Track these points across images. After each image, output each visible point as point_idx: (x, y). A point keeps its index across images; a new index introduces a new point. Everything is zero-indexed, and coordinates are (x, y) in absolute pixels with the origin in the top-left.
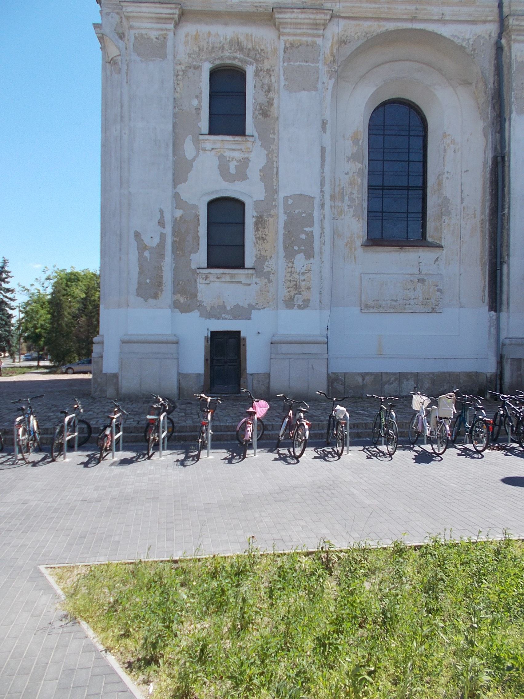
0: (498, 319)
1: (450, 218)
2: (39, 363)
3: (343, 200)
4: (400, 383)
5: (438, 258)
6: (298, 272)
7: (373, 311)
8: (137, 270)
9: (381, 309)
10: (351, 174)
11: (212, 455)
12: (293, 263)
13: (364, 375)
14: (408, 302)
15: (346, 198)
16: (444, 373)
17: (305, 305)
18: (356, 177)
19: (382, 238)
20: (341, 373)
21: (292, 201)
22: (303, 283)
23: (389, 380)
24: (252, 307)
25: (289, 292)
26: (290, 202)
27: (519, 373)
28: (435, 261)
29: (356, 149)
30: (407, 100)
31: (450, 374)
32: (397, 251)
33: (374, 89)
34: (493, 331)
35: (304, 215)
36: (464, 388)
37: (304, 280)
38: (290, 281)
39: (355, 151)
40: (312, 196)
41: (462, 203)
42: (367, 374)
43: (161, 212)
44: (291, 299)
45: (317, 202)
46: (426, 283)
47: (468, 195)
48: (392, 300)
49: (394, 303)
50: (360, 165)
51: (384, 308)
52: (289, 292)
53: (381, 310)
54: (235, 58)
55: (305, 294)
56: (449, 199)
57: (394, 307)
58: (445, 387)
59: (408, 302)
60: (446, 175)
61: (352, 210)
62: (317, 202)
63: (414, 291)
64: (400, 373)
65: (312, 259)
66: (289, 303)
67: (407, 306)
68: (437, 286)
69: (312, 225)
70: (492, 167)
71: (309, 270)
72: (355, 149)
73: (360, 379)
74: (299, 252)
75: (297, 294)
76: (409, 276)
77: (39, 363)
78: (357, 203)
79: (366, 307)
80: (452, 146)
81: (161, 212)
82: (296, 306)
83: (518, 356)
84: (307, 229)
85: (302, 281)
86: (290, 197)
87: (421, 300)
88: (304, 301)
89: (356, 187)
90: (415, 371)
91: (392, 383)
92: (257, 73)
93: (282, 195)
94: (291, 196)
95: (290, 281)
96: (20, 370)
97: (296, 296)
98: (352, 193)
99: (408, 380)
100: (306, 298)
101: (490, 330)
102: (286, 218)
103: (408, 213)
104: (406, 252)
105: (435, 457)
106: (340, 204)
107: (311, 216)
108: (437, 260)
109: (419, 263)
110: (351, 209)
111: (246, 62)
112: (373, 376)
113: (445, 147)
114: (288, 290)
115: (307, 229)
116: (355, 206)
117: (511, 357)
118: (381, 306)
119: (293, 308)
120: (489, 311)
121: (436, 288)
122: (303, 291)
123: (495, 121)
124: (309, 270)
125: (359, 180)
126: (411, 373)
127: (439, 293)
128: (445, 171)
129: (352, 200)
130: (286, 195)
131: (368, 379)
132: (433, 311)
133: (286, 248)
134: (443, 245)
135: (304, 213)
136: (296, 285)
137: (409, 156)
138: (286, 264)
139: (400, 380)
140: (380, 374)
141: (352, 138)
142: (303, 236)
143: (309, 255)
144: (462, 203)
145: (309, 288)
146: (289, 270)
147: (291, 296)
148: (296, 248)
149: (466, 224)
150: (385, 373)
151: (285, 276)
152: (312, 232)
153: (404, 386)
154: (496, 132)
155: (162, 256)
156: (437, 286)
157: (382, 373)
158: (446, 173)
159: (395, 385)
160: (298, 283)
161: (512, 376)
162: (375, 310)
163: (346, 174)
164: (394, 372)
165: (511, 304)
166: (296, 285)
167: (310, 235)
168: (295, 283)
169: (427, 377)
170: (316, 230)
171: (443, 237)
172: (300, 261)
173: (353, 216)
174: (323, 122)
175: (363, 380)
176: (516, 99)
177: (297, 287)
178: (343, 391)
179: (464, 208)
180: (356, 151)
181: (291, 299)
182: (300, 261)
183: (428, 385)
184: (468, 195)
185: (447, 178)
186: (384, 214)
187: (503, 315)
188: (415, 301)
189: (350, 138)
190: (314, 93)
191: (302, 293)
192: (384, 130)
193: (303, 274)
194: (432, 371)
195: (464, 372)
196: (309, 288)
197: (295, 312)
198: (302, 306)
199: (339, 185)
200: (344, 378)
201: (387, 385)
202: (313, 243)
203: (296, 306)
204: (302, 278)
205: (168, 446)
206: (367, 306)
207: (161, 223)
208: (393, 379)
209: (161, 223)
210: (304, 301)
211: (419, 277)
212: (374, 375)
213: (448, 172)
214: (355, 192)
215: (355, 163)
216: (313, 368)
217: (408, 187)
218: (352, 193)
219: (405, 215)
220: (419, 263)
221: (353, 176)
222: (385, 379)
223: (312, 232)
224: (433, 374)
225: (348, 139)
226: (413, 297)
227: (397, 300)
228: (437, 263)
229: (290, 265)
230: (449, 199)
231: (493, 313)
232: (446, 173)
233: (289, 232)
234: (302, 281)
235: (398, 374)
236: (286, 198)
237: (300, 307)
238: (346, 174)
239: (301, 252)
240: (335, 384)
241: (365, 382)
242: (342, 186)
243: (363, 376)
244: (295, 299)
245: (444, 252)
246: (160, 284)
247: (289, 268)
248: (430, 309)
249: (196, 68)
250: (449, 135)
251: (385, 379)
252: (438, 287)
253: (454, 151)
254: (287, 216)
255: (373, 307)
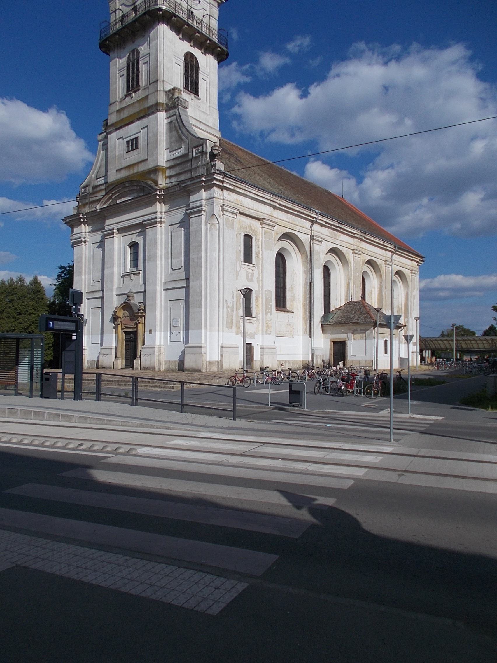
2: (59, 379)
8: (226, 316)
24: (255, 333)
43: (233, 292)
54: (250, 233)
77: (59, 379)
81: (233, 292)
84: (270, 304)
92: (256, 239)
96: (119, 378)
105: (169, 209)
111: (253, 235)
115: (270, 304)
137: (213, 604)
155: (233, 311)
165: (314, 335)
197: (268, 335)
207: (233, 297)
209: (233, 297)
236: (265, 291)
246: (232, 323)
249: (240, 234)
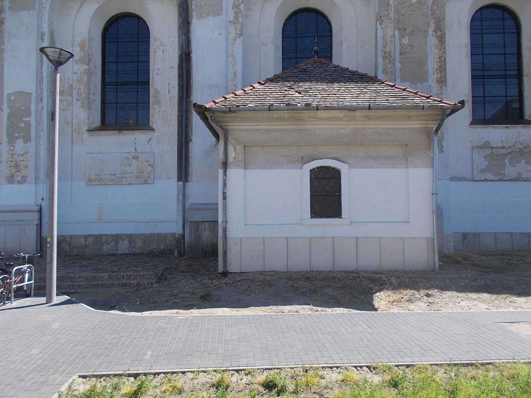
0: (184, 187)
1: (161, 106)
3: (71, 95)
4: (116, 243)
5: (151, 138)
6: (18, 154)
7: (95, 183)
9: (102, 182)
10: (79, 74)
11: (14, 303)
12: (14, 147)
13: (86, 237)
14: (124, 176)
15: (75, 93)
16: (154, 234)
17: (23, 180)
18: (83, 76)
19: (116, 124)
20: (68, 236)
21: (14, 97)
22: (22, 163)
23: (108, 240)
25: (10, 170)
26: (12, 98)
27: (197, 233)
28: (148, 142)
29: (83, 54)
30: (131, 13)
31: (158, 235)
32: (117, 134)
33: (98, 5)
34: (181, 198)
35: (23, 108)
36: (170, 247)
37: (23, 160)
38: (11, 161)
39: (82, 56)
40: (30, 92)
41: (169, 93)
42: (89, 236)
44: (12, 176)
45: (34, 97)
46: (140, 160)
47: (173, 87)
48: (111, 174)
49: (113, 177)
50: (86, 67)
51: (104, 181)
52: (10, 170)
53: (102, 182)
55: (24, 172)
56: (159, 91)
57: (113, 180)
58: (154, 246)
59: (124, 176)
60: (156, 71)
61: (79, 102)
62: (34, 97)
63: (130, 166)
64: (116, 234)
65: (29, 143)
66: (11, 179)
67: (124, 179)
68: (149, 161)
69: (29, 116)
70: (180, 63)
71: (27, 152)
72: (82, 54)
73: (83, 241)
74: (18, 138)
75: (17, 172)
76: (126, 154)
78: (83, 97)
79: (90, 181)
80: (161, 48)
82: (16, 181)
83: (195, 219)
84: (25, 119)
85: (21, 161)
86: (12, 94)
87: (136, 174)
88: (22, 177)
89: (83, 84)
90: (129, 232)
91: (109, 243)
93: (6, 93)
94: (13, 93)
95: (11, 161)
97: (16, 173)
98: (79, 89)
99: (123, 240)
100: (24, 175)
101: (178, 197)
102: (9, 111)
103: (137, 103)
104: (124, 134)
106: (69, 98)
107: (29, 108)
108: (150, 140)
109: (135, 143)
110: (79, 102)
112: (94, 238)
113: (155, 48)
114: (10, 168)
115: (25, 119)
116: (82, 99)
117: (189, 220)
118: (102, 180)
119: (13, 183)
120: (177, 181)
121: (148, 164)
122: (22, 169)
123: (182, 26)
124: (27, 152)
125: (86, 78)
126: (126, 235)
127: (150, 168)
128: (156, 69)
129: (79, 94)
130: (9, 92)
131: (90, 240)
132: (145, 182)
133: (8, 135)
134: (155, 128)
135: (24, 106)
136: (16, 164)
138: (8, 148)
139: (116, 241)
140: (99, 236)
141: (79, 45)
142: (22, 125)
143: (27, 140)
144: (169, 93)
145: (26, 167)
146: (11, 152)
147: (12, 174)
148: (17, 135)
149: (172, 110)
150: (104, 235)
151: (8, 158)
152: (29, 121)
153: (119, 246)
154: (182, 34)
156: (149, 161)
157: (101, 235)
158: (156, 70)
159: (112, 244)
160: (18, 163)
161: (191, 234)
162: (97, 183)
163: (75, 74)
164: (112, 234)
166: (16, 164)
167: (28, 124)
168: (15, 163)
169: (139, 237)
170: (33, 119)
171: (154, 121)
172: (20, 145)
173: (80, 107)
174: (42, 34)
175: (86, 241)
176: (196, 6)
177: (17, 166)
178: (69, 251)
179: (170, 97)
180: (83, 55)
181: (12, 176)
182: (20, 145)
183: (140, 245)
184: (173, 87)
185: (157, 74)
186: (118, 105)
187: (189, 185)
188: (130, 175)
189: (78, 46)
190: (32, 12)
191: (21, 171)
192: (118, 38)
193: (22, 155)
194: (144, 233)
195: (170, 233)
196: (26, 167)
197: (16, 187)
198: (21, 181)
199: (68, 83)
200: (70, 240)
201: (105, 245)
202: (30, 130)
203: (16, 181)
204: (21, 159)
205: (14, 295)
206: (90, 180)
208: (110, 240)
210: (22, 177)
211: (134, 155)
212: (95, 236)
213: (158, 69)
214: (82, 88)
215: (82, 65)
216: (24, 232)
217: (138, 82)
218: (79, 89)
219: (115, 105)
220: (135, 143)
221: (81, 75)
222: (104, 240)
223: (29, 121)
224: (144, 235)
225: (76, 47)
226: (129, 171)
227: (115, 174)
228: (150, 143)
229: (12, 148)
230: (159, 91)
231: (181, 183)
232: (156, 70)
233: (11, 122)
234: (21, 161)
235: (115, 236)
236: (9, 95)
237: (19, 182)
238: (75, 74)
239: (21, 138)
240: (63, 245)
241: (87, 242)
242: (71, 83)
243: (85, 238)
244: (16, 176)
245: (156, 133)
247: (11, 150)
248: (143, 181)
250: (159, 39)
251: (104, 240)
252: (150, 163)
253: (163, 52)
254: (10, 110)
255: (95, 181)
